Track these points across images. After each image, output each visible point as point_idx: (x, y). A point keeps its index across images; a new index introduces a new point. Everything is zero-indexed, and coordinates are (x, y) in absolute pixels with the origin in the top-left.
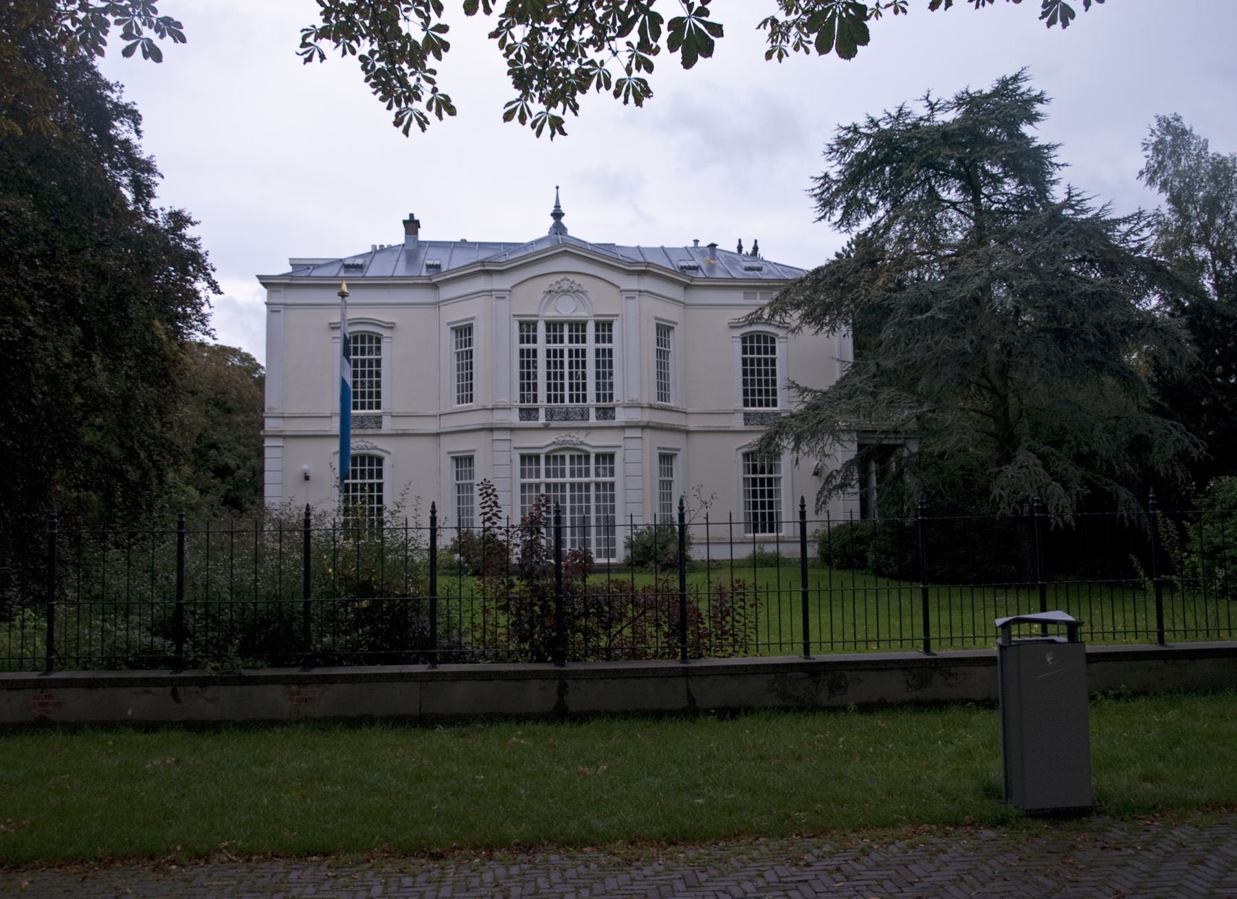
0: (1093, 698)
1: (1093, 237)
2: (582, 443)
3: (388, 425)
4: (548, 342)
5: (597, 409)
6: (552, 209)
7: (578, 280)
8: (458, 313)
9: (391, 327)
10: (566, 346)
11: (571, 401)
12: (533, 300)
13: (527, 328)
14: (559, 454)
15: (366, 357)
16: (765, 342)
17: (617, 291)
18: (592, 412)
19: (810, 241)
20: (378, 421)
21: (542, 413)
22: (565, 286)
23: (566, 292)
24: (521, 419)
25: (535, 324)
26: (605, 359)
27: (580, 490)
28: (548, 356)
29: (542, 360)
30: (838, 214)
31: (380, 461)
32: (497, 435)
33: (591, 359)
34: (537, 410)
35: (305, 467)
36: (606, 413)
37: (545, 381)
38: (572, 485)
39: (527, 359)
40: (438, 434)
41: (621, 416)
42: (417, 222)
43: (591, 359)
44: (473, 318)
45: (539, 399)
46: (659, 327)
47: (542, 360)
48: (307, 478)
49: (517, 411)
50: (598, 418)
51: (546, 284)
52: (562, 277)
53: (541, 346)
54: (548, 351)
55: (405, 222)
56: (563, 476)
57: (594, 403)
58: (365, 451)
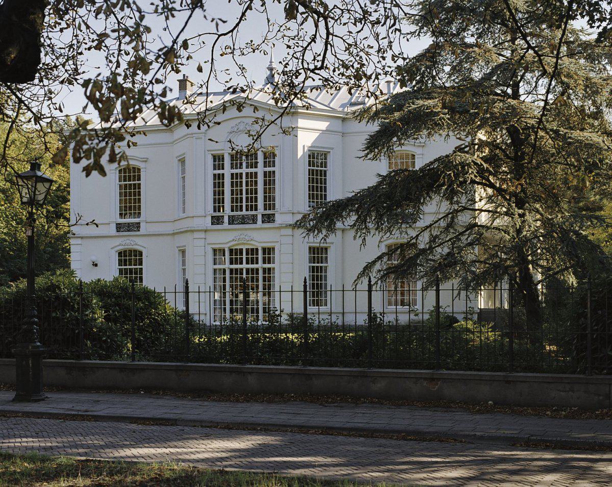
3: (143, 229)
4: (215, 169)
8: (180, 149)
10: (244, 170)
11: (247, 210)
13: (218, 160)
14: (238, 247)
15: (132, 182)
16: (134, 172)
20: (138, 226)
24: (212, 224)
26: (270, 179)
27: (236, 274)
28: (232, 178)
29: (227, 181)
31: (141, 254)
32: (196, 235)
33: (260, 179)
36: (269, 219)
37: (230, 196)
38: (247, 270)
39: (218, 180)
41: (279, 219)
43: (260, 179)
44: (184, 154)
45: (259, 207)
46: (214, 157)
47: (227, 181)
48: (96, 265)
49: (210, 218)
50: (263, 222)
52: (239, 120)
53: (227, 171)
54: (232, 174)
56: (241, 263)
58: (130, 247)
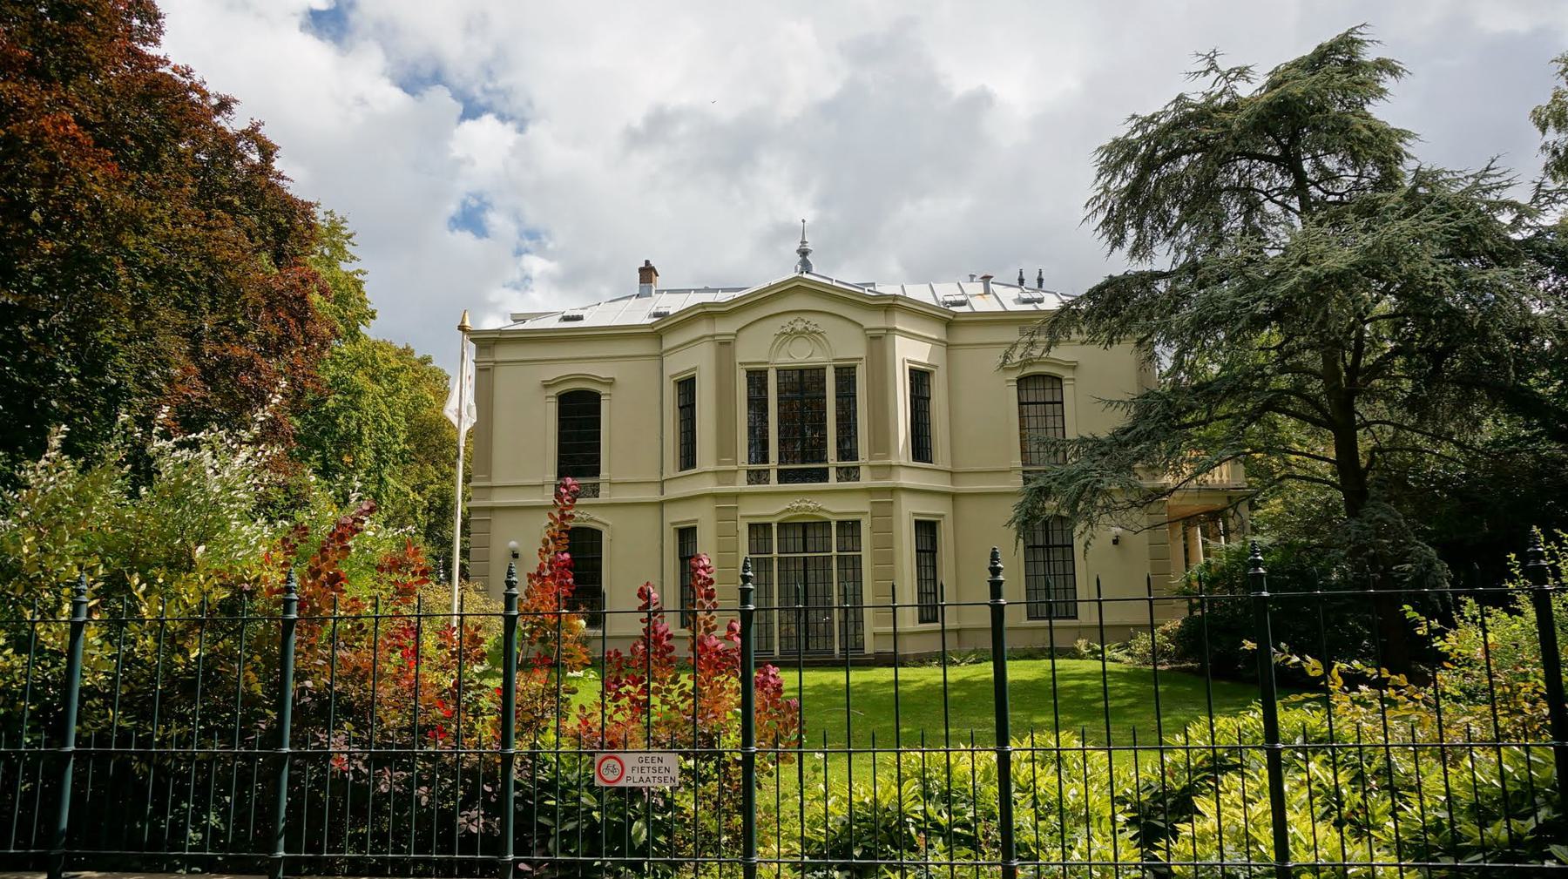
0: (972, 276)
1: (1470, 232)
2: (820, 509)
5: (838, 469)
6: (798, 245)
7: (814, 319)
8: (677, 365)
9: (610, 383)
12: (764, 348)
17: (859, 331)
18: (774, 475)
19: (1090, 259)
21: (832, 473)
22: (799, 326)
23: (800, 334)
25: (765, 372)
30: (1131, 234)
34: (768, 471)
35: (513, 544)
40: (661, 503)
42: (653, 269)
51: (775, 326)
52: (795, 317)
55: (641, 270)
57: (746, 465)
